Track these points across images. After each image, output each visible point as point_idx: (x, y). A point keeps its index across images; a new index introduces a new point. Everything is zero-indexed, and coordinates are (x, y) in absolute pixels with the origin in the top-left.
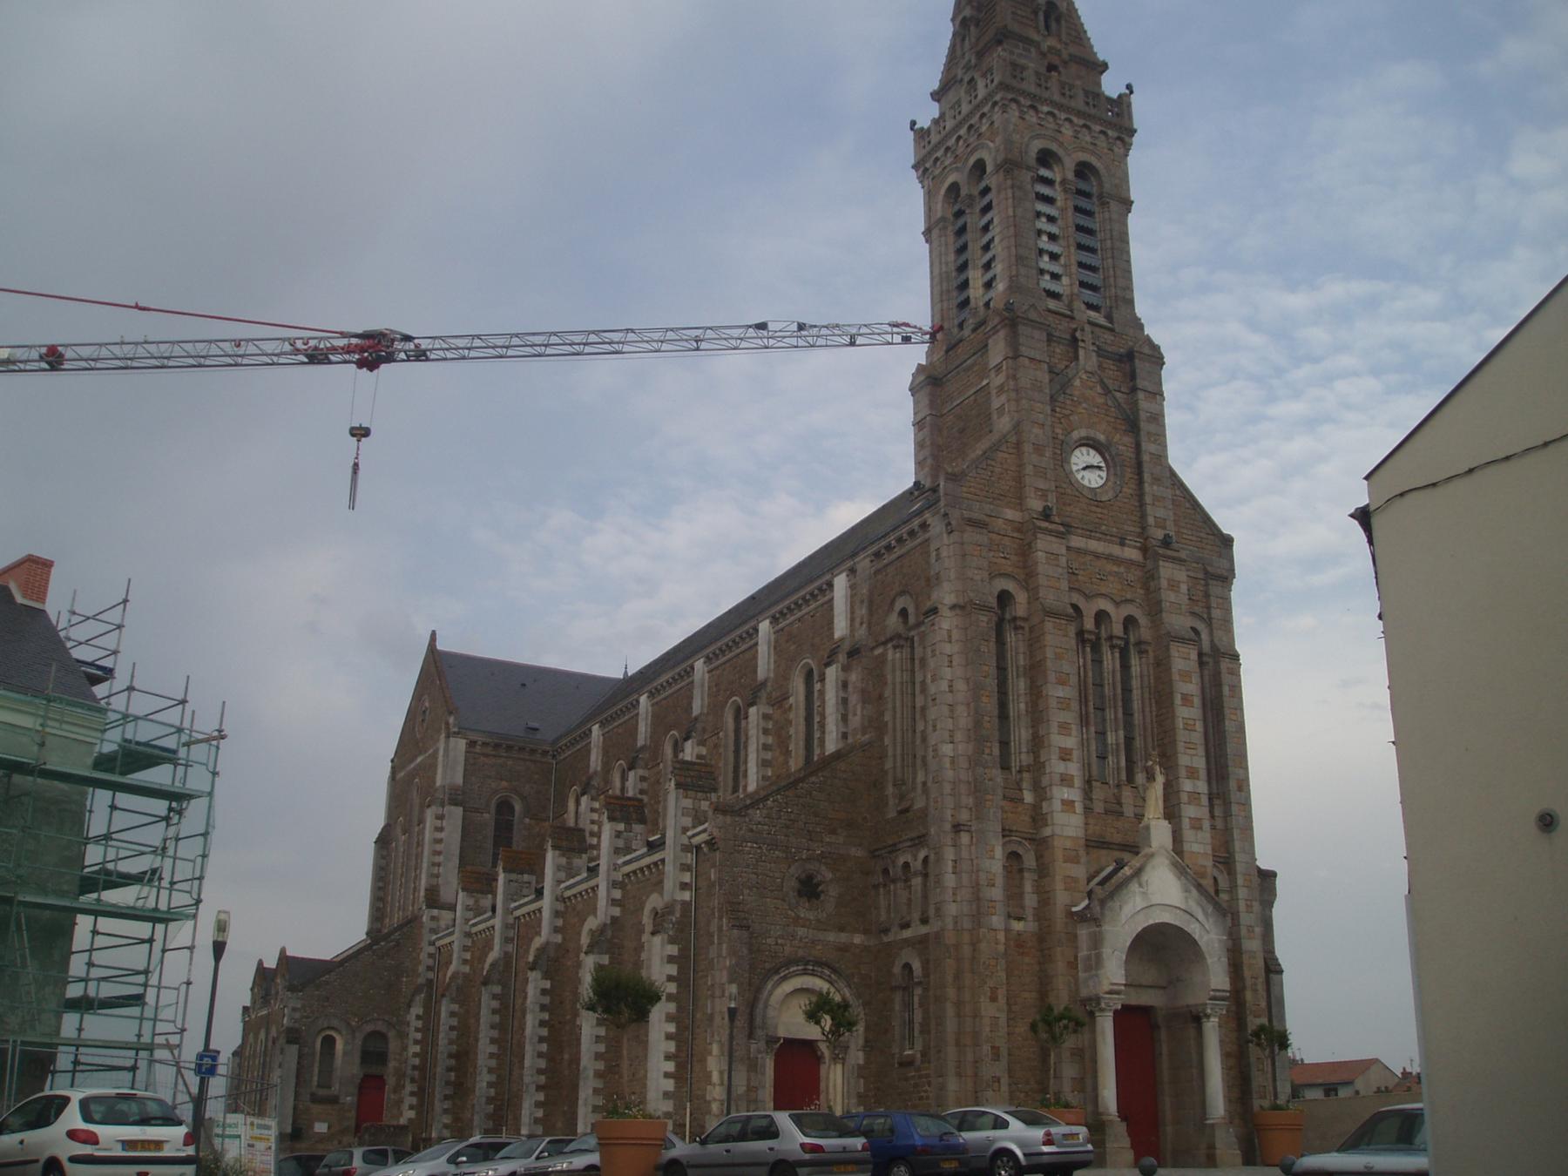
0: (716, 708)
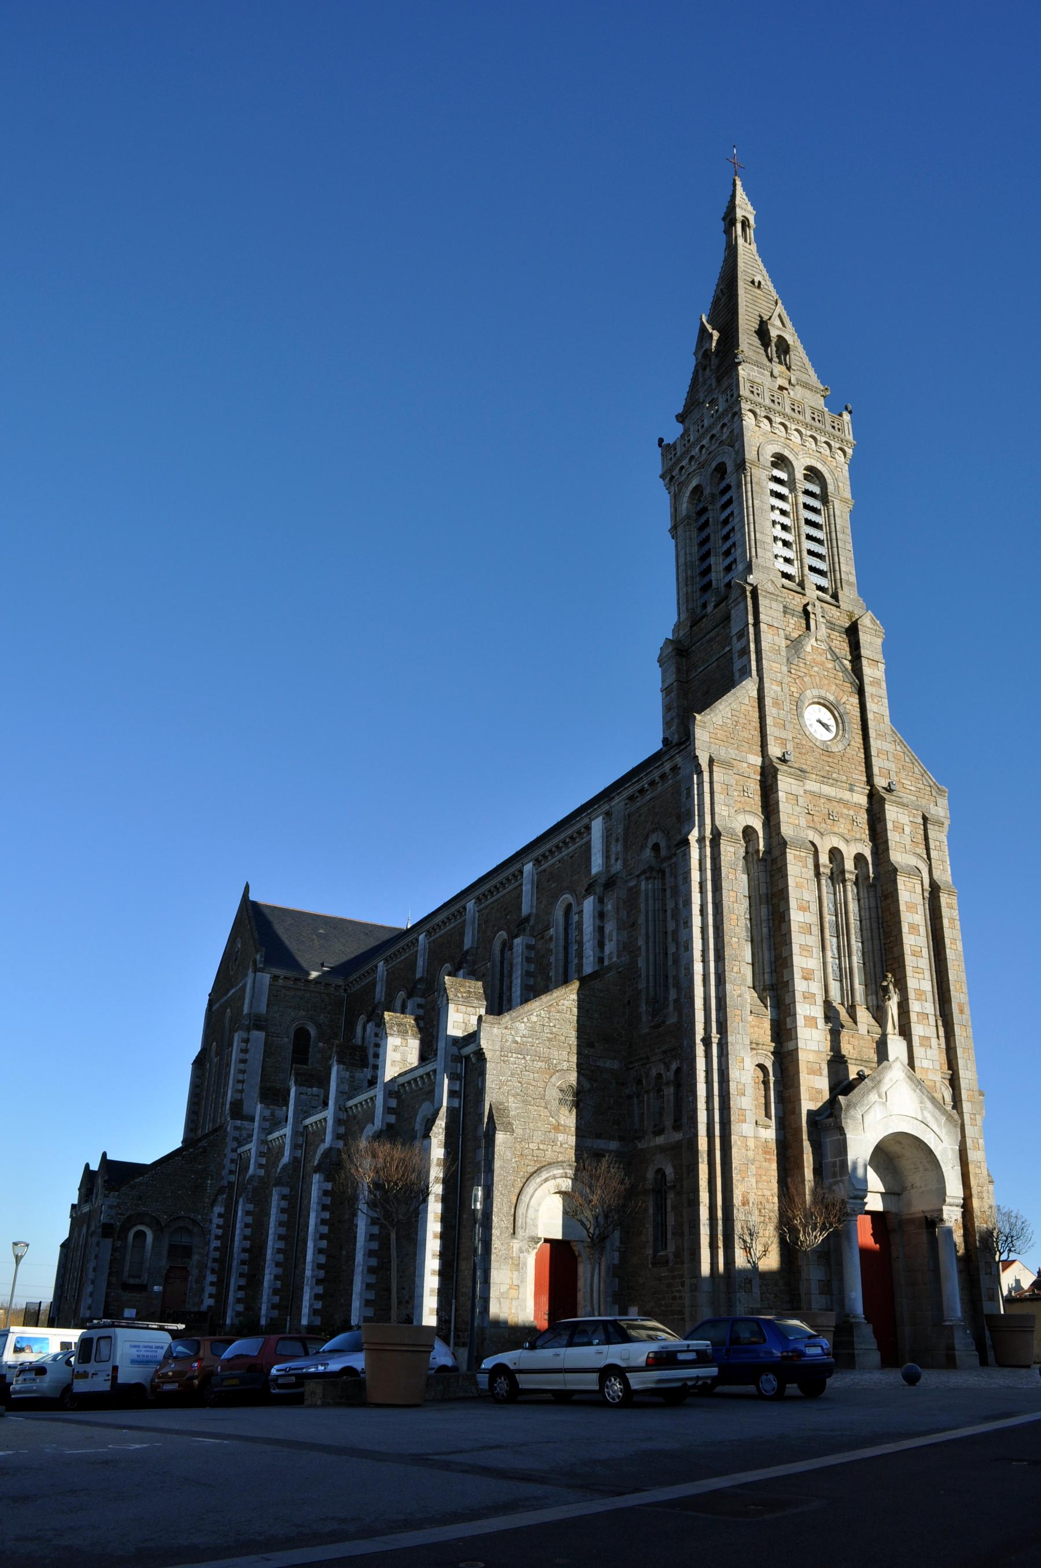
0: (484, 940)
